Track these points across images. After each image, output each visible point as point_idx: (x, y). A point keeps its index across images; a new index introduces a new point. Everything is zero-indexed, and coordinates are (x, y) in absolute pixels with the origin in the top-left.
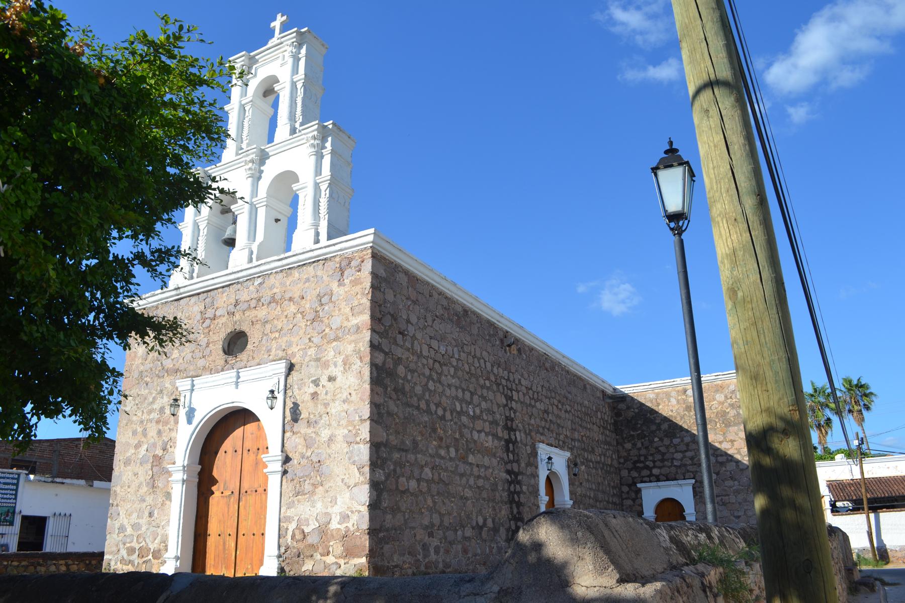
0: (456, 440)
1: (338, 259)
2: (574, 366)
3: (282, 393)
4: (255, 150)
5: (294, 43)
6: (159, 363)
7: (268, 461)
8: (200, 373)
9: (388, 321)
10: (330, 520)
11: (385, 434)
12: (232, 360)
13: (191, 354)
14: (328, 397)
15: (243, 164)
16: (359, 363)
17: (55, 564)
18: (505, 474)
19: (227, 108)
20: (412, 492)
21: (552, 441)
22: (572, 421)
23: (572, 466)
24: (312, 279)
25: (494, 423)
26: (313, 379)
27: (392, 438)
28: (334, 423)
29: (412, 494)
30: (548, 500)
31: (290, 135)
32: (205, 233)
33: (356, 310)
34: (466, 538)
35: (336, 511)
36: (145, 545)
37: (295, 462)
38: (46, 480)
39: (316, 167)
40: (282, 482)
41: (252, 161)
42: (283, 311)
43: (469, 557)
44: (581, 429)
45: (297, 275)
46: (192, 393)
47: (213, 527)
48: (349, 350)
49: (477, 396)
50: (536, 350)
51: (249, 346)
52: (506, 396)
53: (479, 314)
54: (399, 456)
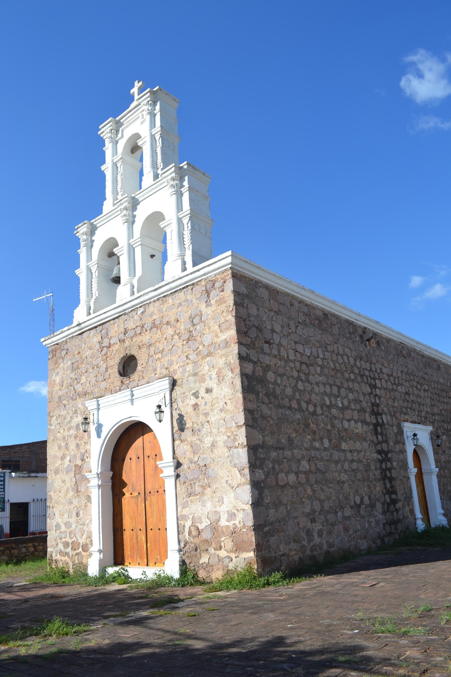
0: (328, 431)
1: (203, 283)
2: (428, 350)
3: (169, 406)
4: (127, 198)
5: (150, 102)
6: (72, 388)
7: (163, 467)
8: (103, 394)
9: (253, 333)
10: (220, 518)
11: (261, 436)
12: (126, 381)
13: (95, 378)
14: (208, 407)
15: (119, 212)
16: (231, 375)
17: (25, 547)
18: (376, 455)
19: (103, 168)
20: (291, 485)
21: (415, 418)
22: (431, 398)
23: (435, 438)
24: (184, 303)
25: (362, 410)
26: (193, 392)
27: (268, 439)
28: (215, 431)
29: (292, 487)
30: (416, 471)
31: (154, 181)
32: (97, 275)
33: (224, 326)
34: (346, 517)
35: (224, 509)
36: (76, 540)
37: (185, 466)
38: (24, 476)
39: (178, 204)
40: (176, 485)
41: (126, 208)
42: (162, 334)
43: (350, 534)
44: (439, 404)
45: (171, 301)
46: (98, 411)
47: (127, 523)
48: (221, 363)
49: (344, 389)
50: (393, 341)
51: (139, 368)
52: (370, 385)
53: (338, 315)
54: (276, 455)
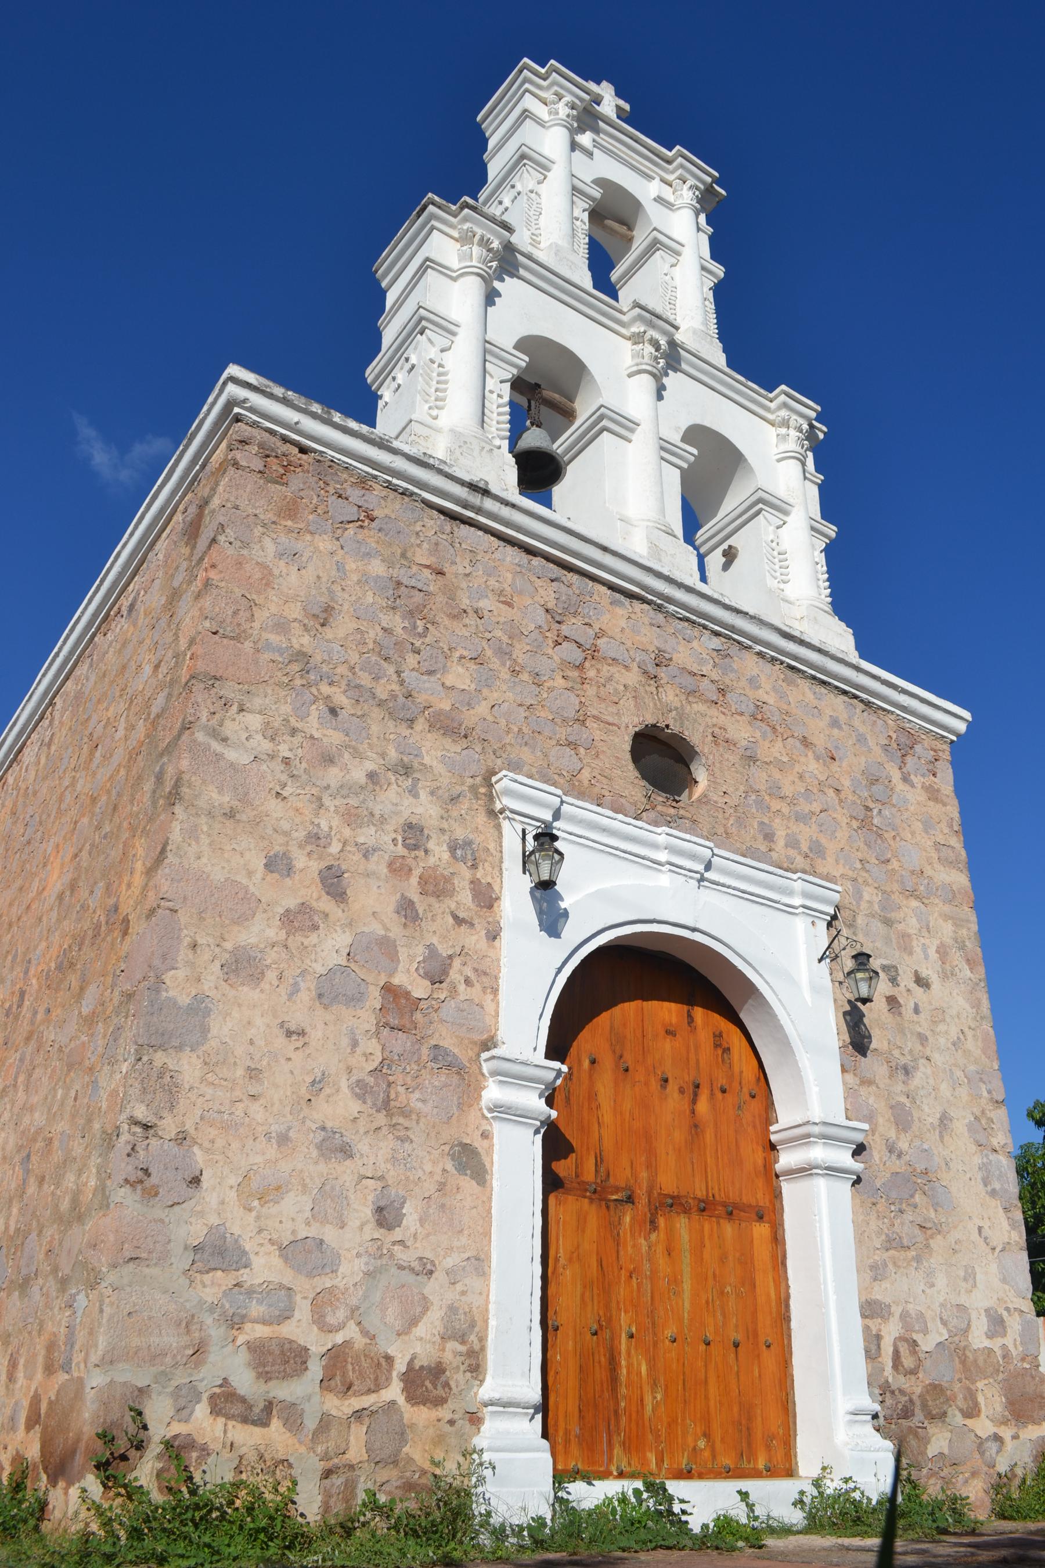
10: (969, 1325)
35: (979, 1301)
